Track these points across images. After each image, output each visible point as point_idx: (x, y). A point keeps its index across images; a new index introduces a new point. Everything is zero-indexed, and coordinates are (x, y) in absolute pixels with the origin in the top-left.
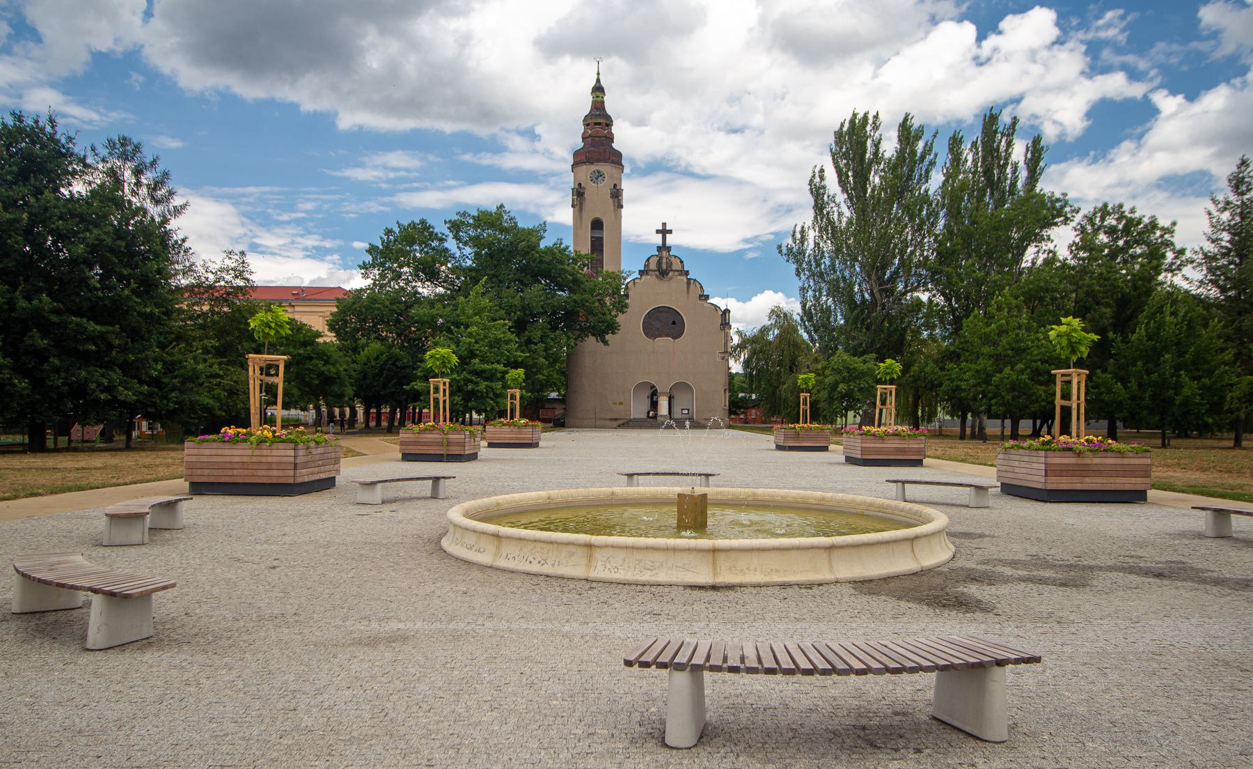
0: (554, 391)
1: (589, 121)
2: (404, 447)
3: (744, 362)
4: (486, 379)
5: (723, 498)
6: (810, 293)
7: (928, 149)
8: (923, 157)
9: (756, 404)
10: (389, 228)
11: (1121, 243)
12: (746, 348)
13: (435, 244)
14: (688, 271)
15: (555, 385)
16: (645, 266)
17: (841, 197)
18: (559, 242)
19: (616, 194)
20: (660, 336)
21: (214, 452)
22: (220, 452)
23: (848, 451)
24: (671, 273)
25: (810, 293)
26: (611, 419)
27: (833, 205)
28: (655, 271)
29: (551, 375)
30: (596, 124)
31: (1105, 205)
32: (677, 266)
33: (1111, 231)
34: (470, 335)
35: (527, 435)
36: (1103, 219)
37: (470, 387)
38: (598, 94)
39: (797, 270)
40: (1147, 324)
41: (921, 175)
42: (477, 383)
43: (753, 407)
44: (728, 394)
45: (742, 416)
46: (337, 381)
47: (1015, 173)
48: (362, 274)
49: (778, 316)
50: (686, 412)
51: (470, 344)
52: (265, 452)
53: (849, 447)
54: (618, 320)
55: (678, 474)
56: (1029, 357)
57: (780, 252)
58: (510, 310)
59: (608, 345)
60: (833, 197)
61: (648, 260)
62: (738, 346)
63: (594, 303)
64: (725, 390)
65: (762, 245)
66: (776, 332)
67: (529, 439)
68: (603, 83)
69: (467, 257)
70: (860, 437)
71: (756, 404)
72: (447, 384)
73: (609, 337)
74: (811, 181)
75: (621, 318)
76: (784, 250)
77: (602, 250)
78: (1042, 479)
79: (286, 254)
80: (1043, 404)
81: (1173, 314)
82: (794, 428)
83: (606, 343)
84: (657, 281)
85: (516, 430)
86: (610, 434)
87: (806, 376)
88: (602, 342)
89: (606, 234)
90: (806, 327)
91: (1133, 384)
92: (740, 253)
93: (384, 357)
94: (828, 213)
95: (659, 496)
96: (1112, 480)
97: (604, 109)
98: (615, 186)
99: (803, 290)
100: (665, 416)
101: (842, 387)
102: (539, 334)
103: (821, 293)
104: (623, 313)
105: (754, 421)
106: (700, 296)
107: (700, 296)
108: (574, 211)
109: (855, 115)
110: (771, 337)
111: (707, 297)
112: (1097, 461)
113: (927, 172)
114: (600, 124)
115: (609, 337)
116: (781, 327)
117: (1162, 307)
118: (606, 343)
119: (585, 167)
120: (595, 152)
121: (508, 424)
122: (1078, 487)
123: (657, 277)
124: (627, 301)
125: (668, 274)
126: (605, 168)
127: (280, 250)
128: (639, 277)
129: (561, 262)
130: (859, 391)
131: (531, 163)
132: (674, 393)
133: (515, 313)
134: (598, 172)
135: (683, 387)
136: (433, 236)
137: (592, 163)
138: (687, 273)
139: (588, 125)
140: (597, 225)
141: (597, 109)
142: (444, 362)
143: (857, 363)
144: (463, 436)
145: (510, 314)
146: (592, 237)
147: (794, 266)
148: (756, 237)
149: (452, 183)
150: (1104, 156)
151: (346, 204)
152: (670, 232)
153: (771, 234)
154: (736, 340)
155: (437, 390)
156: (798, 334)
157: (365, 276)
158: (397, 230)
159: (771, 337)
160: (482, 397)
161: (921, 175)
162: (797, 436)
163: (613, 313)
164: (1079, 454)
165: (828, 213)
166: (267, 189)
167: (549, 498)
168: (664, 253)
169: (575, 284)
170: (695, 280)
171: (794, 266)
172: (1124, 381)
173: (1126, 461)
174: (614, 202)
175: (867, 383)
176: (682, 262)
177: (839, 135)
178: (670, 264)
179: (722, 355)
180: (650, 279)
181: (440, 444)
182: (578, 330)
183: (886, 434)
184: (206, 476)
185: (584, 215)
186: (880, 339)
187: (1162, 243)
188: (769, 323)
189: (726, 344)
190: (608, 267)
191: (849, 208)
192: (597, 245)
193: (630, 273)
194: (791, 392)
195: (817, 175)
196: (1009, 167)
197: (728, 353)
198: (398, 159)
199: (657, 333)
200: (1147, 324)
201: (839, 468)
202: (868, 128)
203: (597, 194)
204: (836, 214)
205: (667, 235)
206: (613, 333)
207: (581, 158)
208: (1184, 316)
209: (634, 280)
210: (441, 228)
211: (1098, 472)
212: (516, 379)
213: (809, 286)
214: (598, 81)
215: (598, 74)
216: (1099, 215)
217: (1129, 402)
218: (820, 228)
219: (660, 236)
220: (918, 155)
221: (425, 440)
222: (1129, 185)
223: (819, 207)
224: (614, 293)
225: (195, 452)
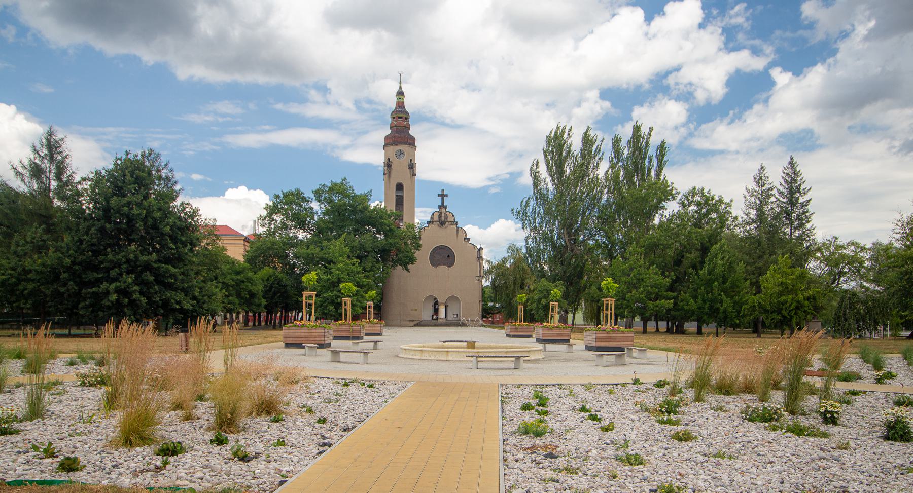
6: (531, 240)
7: (598, 150)
10: (277, 194)
11: (704, 210)
16: (431, 218)
17: (549, 179)
20: (440, 265)
21: (294, 331)
22: (297, 331)
24: (447, 223)
25: (531, 240)
26: (410, 321)
30: (399, 117)
31: (694, 188)
32: (450, 219)
33: (698, 204)
34: (338, 269)
35: (377, 328)
36: (693, 196)
38: (401, 97)
40: (709, 264)
41: (594, 166)
43: (497, 313)
47: (650, 163)
51: (339, 274)
52: (313, 331)
54: (415, 255)
56: (644, 284)
57: (513, 213)
59: (409, 272)
61: (433, 214)
65: (501, 183)
67: (379, 331)
68: (403, 89)
73: (409, 266)
75: (417, 254)
78: (595, 342)
80: (652, 311)
81: (723, 259)
83: (408, 270)
84: (439, 228)
85: (372, 325)
89: (405, 194)
91: (699, 300)
92: (485, 189)
93: (272, 279)
94: (541, 189)
96: (619, 343)
97: (404, 107)
98: (411, 160)
102: (370, 265)
106: (465, 239)
107: (465, 239)
109: (558, 128)
110: (508, 265)
111: (469, 239)
112: (614, 335)
113: (598, 164)
114: (401, 117)
115: (409, 266)
117: (716, 255)
118: (408, 270)
119: (392, 147)
120: (398, 137)
122: (608, 345)
123: (438, 226)
126: (405, 148)
129: (381, 218)
131: (328, 112)
132: (449, 304)
134: (400, 151)
135: (454, 299)
137: (397, 145)
138: (457, 223)
139: (394, 118)
140: (400, 187)
141: (400, 107)
145: (352, 252)
146: (396, 196)
148: (497, 176)
149: (267, 127)
150: (740, 118)
151: (185, 143)
152: (446, 196)
153: (507, 173)
154: (486, 266)
155: (346, 304)
158: (282, 196)
159: (508, 265)
161: (594, 166)
162: (516, 330)
163: (413, 251)
164: (608, 332)
166: (123, 129)
168: (443, 210)
169: (389, 233)
172: (695, 298)
173: (625, 335)
176: (453, 216)
177: (548, 139)
178: (446, 217)
181: (349, 331)
182: (391, 261)
183: (554, 327)
184: (291, 341)
185: (391, 180)
187: (726, 212)
190: (406, 219)
192: (400, 201)
196: (647, 158)
198: (226, 107)
200: (709, 264)
202: (565, 136)
203: (400, 165)
206: (412, 264)
207: (390, 141)
208: (728, 260)
210: (308, 194)
211: (615, 339)
212: (371, 297)
214: (400, 87)
216: (691, 194)
217: (698, 310)
222: (759, 140)
225: (287, 331)
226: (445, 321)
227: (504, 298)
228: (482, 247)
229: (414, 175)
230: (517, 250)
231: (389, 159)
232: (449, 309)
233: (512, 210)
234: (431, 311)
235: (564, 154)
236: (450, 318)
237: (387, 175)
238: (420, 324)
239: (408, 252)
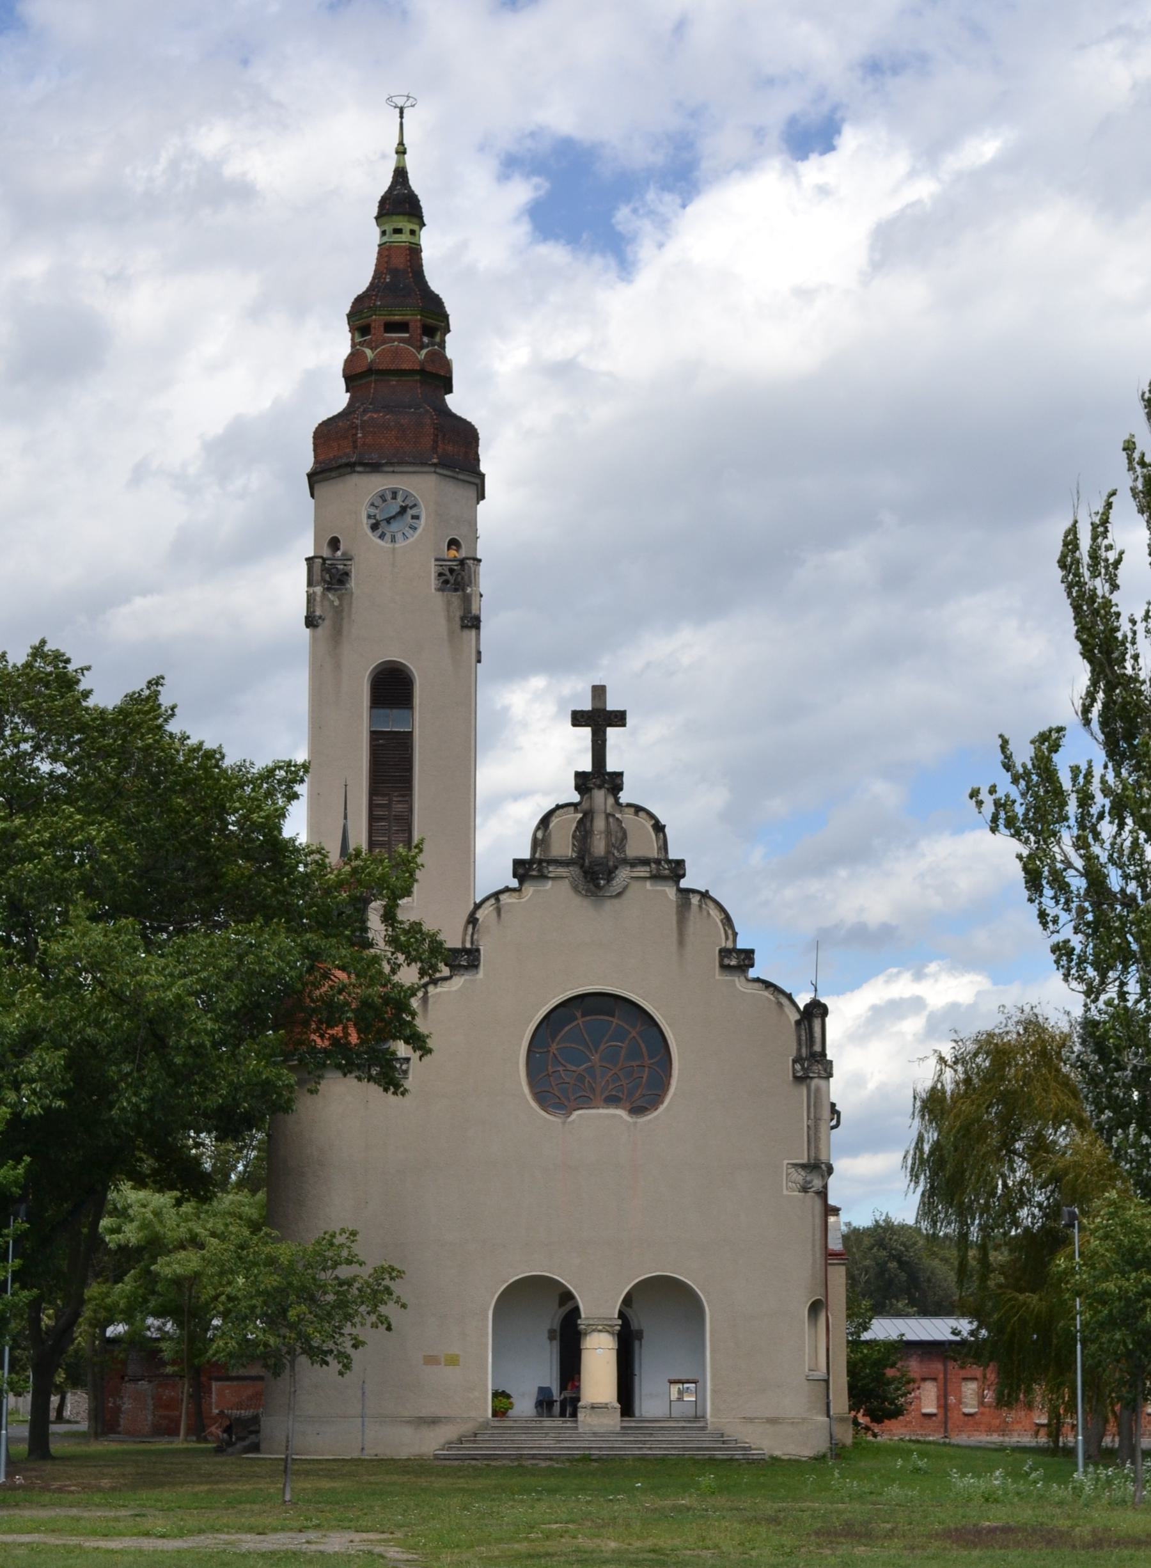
14: (680, 863)
16: (536, 843)
20: (585, 1102)
24: (623, 874)
32: (641, 844)
61: (545, 821)
100: (605, 1406)
106: (725, 953)
107: (725, 953)
108: (314, 640)
111: (747, 958)
125: (610, 875)
128: (514, 883)
137: (375, 468)
146: (373, 733)
152: (619, 718)
168: (600, 796)
170: (705, 895)
176: (659, 828)
209: (496, 895)
214: (401, 175)
215: (401, 151)
229: (472, 622)
231: (334, 543)
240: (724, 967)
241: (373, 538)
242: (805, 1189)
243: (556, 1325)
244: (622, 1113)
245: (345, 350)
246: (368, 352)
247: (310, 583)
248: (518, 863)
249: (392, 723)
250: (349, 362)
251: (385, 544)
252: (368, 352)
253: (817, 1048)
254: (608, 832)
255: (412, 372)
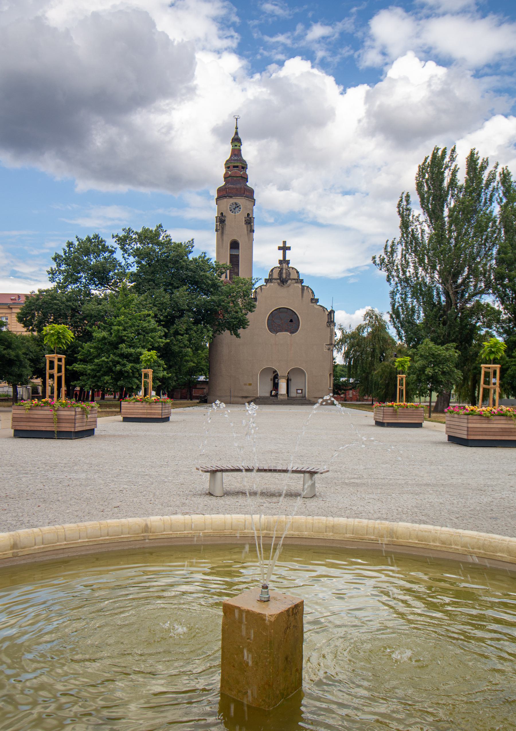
0: (201, 375)
1: (228, 165)
2: (16, 424)
3: (345, 353)
4: (130, 361)
5: (337, 537)
6: (398, 295)
8: (487, 185)
9: (353, 387)
12: (346, 342)
13: (107, 254)
14: (302, 280)
15: (203, 370)
16: (270, 275)
18: (203, 256)
19: (249, 221)
20: (281, 331)
23: (452, 430)
24: (289, 281)
25: (398, 295)
27: (417, 223)
28: (277, 279)
29: (200, 363)
30: (234, 167)
32: (294, 276)
34: (119, 324)
37: (118, 368)
38: (236, 143)
39: (388, 276)
41: (486, 199)
42: (124, 365)
43: (351, 389)
44: (332, 378)
45: (342, 396)
46: (18, 363)
48: (50, 278)
49: (371, 317)
50: (300, 391)
51: (118, 331)
53: (452, 426)
54: (247, 317)
55: (275, 471)
58: (162, 306)
59: (240, 337)
60: (417, 217)
61: (272, 270)
62: (341, 340)
63: (229, 303)
64: (330, 375)
66: (370, 330)
67: (158, 414)
68: (240, 136)
69: (130, 265)
70: (466, 417)
71: (353, 387)
72: (63, 360)
74: (399, 205)
75: (250, 316)
76: (378, 261)
77: (238, 265)
79: (35, 278)
82: (392, 406)
83: (238, 336)
85: (147, 405)
86: (239, 409)
87: (402, 359)
88: (235, 334)
89: (242, 252)
90: (395, 323)
95: (227, 532)
97: (241, 155)
98: (248, 215)
99: (393, 294)
100: (284, 394)
101: (429, 371)
103: (406, 295)
104: (251, 311)
105: (351, 399)
106: (312, 299)
107: (312, 299)
108: (217, 235)
111: (317, 301)
114: (237, 167)
115: (240, 331)
116: (373, 326)
118: (238, 336)
119: (225, 200)
121: (141, 401)
124: (255, 303)
125: (287, 281)
126: (241, 201)
127: (31, 275)
128: (265, 284)
129: (204, 270)
130: (442, 374)
133: (165, 310)
134: (236, 204)
135: (298, 371)
136: (105, 249)
137: (231, 197)
138: (302, 281)
139: (229, 167)
140: (235, 245)
141: (235, 155)
142: (59, 338)
143: (440, 350)
144: (73, 413)
145: (161, 311)
146: (230, 255)
147: (386, 274)
152: (289, 248)
154: (339, 335)
155: (146, 376)
156: (386, 332)
157: (52, 280)
158: (76, 243)
159: (365, 334)
160: (128, 377)
162: (395, 413)
165: (413, 231)
167: (15, 546)
168: (284, 265)
170: (308, 287)
171: (386, 274)
174: (247, 227)
175: (449, 367)
176: (298, 272)
178: (288, 274)
179: (327, 347)
180: (274, 285)
181: (50, 420)
186: (454, 333)
188: (364, 322)
189: (331, 338)
190: (242, 274)
191: (429, 227)
192: (235, 260)
193: (258, 280)
194: (381, 376)
195: (404, 200)
197: (332, 345)
199: (278, 328)
201: (441, 448)
202: (447, 159)
204: (419, 231)
205: (287, 251)
206: (244, 328)
209: (261, 286)
210: (111, 242)
213: (397, 290)
214: (237, 133)
215: (237, 128)
218: (406, 243)
219: (281, 252)
220: (484, 182)
221: (36, 416)
223: (405, 225)
224: (244, 296)
226: (286, 398)
227: (359, 372)
228: (334, 309)
230: (376, 316)
231: (222, 214)
232: (292, 384)
233: (374, 258)
234: (269, 386)
235: (446, 183)
236: (293, 394)
237: (220, 232)
238: (259, 401)
239: (237, 312)
240: (312, 302)
241: (231, 213)
242: (329, 350)
243: (272, 378)
244: (288, 333)
245: (225, 172)
246: (230, 173)
247: (216, 222)
248: (266, 280)
249: (234, 252)
250: (225, 174)
251: (233, 214)
252: (230, 173)
253: (332, 320)
254: (286, 273)
255: (239, 177)
